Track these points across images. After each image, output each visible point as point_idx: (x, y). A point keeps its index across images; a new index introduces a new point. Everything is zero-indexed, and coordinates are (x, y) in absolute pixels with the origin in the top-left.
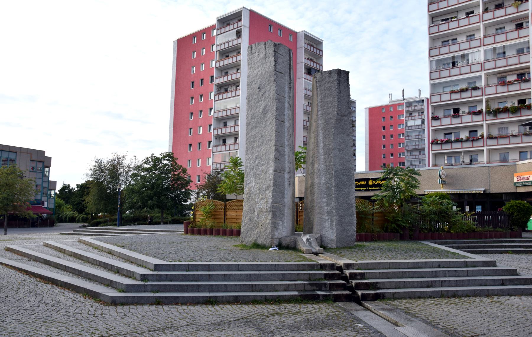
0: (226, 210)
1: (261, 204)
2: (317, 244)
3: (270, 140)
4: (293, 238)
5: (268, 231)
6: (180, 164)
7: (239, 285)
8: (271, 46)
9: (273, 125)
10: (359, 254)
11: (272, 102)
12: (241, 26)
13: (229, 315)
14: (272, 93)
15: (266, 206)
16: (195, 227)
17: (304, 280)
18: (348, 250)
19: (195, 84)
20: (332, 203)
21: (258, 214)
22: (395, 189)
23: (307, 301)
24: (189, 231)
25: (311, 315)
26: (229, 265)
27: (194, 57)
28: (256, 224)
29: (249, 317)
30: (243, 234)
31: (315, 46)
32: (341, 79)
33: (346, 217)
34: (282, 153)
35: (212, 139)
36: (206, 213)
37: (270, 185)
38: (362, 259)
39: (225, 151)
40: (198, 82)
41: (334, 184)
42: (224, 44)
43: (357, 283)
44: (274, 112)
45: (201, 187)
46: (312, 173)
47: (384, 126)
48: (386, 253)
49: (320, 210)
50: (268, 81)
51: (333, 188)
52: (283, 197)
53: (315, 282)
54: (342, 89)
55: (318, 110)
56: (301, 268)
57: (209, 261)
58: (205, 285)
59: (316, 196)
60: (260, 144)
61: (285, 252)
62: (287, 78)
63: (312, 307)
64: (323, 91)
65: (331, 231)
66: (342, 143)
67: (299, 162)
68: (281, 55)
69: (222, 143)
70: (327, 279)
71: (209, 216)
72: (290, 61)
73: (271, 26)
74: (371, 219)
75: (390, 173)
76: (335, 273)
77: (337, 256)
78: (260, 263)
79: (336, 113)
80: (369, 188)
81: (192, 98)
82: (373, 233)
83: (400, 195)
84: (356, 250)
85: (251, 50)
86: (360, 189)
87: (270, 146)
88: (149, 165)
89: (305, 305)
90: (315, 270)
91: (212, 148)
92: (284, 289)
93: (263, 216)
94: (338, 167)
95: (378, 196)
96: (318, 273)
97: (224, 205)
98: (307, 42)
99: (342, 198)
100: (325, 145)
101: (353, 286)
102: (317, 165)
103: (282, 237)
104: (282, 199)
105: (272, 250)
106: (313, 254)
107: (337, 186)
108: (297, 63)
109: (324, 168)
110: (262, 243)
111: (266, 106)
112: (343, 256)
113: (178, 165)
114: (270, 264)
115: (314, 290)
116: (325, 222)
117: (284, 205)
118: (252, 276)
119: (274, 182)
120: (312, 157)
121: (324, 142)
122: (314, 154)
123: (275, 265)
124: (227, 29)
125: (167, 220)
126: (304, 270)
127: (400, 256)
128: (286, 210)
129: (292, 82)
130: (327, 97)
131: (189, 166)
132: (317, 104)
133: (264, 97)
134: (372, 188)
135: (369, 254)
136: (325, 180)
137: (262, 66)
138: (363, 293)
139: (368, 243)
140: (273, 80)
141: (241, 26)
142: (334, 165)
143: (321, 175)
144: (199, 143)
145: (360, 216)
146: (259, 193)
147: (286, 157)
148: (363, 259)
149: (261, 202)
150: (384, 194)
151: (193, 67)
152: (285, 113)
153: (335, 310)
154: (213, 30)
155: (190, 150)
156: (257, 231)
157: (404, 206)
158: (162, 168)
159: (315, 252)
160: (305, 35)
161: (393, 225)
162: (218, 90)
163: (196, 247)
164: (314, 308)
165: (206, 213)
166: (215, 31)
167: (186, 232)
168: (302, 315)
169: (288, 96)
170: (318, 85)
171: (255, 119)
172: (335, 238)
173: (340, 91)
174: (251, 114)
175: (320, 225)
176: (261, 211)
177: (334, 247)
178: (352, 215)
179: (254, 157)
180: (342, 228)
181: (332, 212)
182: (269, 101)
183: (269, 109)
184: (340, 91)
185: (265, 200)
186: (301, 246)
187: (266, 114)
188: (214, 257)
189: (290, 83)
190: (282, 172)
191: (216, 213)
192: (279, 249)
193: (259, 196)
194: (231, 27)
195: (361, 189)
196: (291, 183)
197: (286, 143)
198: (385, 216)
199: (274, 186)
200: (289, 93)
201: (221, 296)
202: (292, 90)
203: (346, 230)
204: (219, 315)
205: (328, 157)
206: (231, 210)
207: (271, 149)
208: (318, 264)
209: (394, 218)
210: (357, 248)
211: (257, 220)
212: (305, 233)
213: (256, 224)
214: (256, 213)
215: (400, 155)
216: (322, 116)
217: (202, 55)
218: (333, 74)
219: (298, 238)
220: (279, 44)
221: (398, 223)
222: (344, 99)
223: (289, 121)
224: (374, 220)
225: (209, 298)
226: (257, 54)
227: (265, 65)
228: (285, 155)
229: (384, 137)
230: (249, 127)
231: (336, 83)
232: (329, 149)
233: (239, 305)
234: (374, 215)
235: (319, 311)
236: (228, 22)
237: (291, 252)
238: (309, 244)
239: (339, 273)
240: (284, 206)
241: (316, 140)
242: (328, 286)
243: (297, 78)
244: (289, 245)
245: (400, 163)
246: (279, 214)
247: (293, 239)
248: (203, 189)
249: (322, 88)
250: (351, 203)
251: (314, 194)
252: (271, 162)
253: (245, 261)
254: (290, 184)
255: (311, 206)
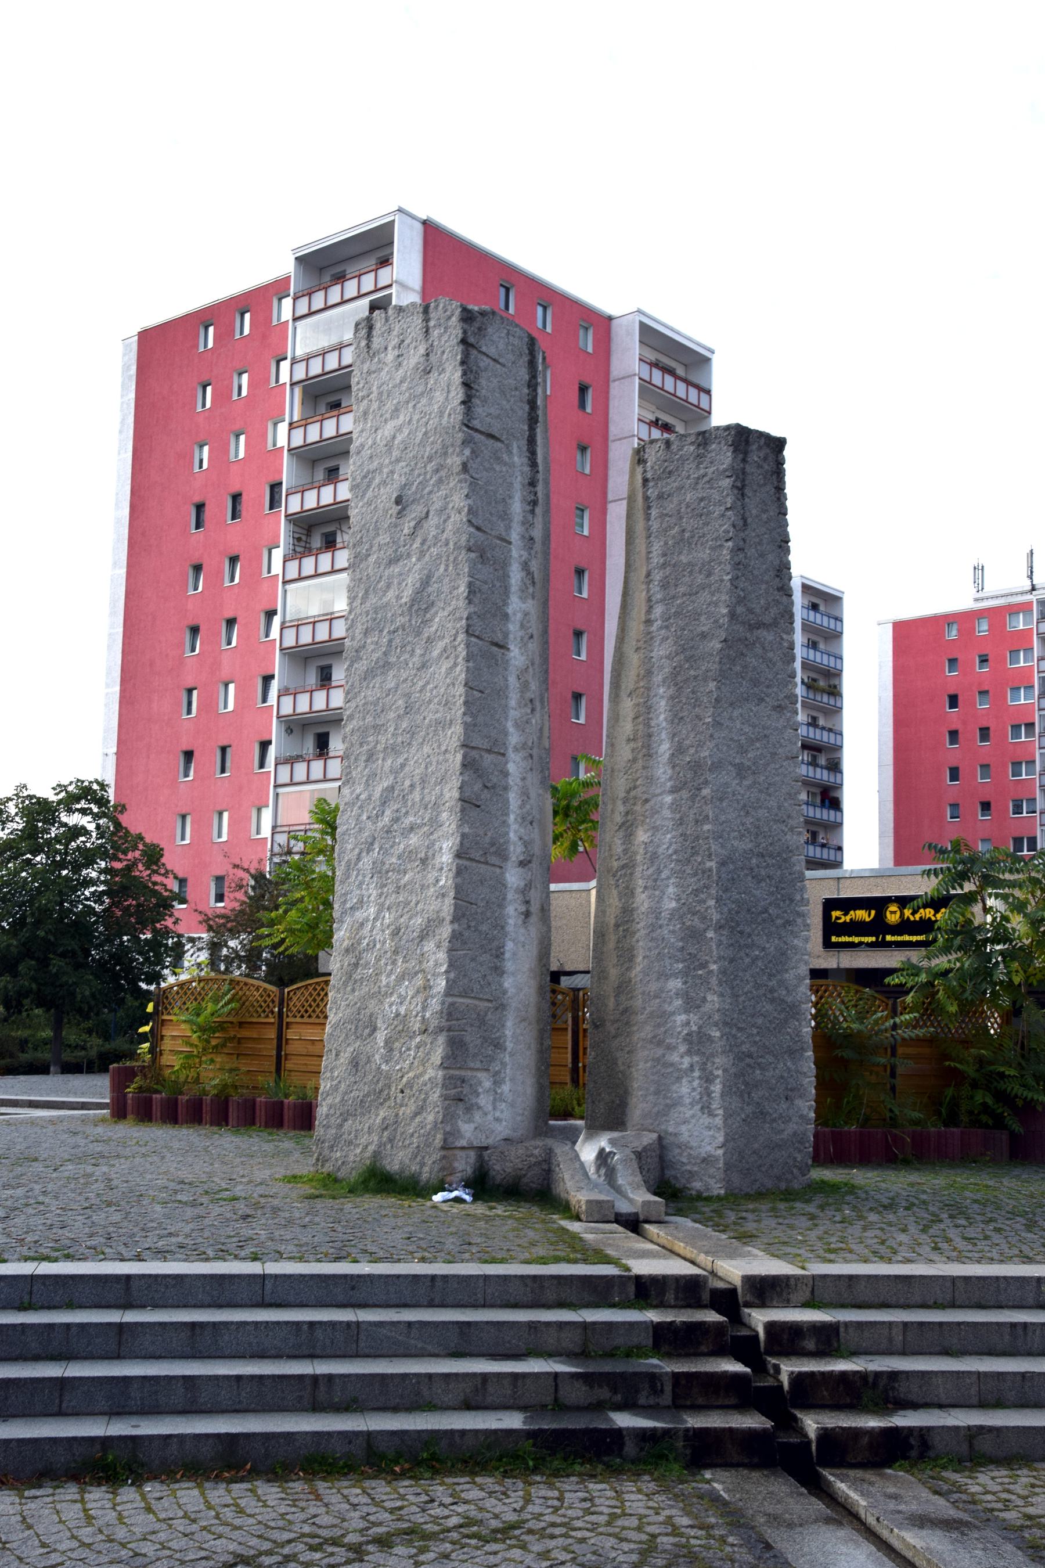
0: (286, 1020)
1: (400, 996)
2: (639, 1178)
3: (442, 724)
4: (536, 1147)
5: (431, 1118)
6: (134, 830)
7: (252, 1377)
8: (449, 318)
9: (457, 657)
10: (819, 1231)
11: (451, 559)
12: (390, 286)
13: (174, 1545)
14: (455, 522)
15: (424, 1008)
16: (157, 1092)
17: (561, 1355)
18: (773, 1209)
19: (208, 513)
20: (709, 998)
21: (386, 1042)
22: (986, 941)
23: (565, 1459)
24: (129, 1108)
25: (565, 1549)
26: (223, 1277)
27: (204, 405)
28: (380, 1085)
29: (269, 1553)
30: (327, 1127)
31: (680, 371)
32: (748, 469)
33: (771, 1059)
34: (495, 780)
35: (275, 732)
36: (202, 1029)
37: (442, 915)
38: (830, 1254)
39: (325, 780)
40: (219, 508)
41: (716, 917)
42: (323, 354)
43: (800, 1374)
44: (462, 603)
45: (222, 921)
46: (623, 867)
47: (952, 692)
48: (942, 1226)
49: (659, 1025)
50: (437, 471)
51: (710, 934)
52: (499, 971)
53: (608, 1367)
54: (754, 512)
55: (649, 600)
56: (550, 1296)
57: (139, 1258)
58: (93, 1379)
59: (638, 969)
60: (400, 739)
61: (500, 1210)
62: (518, 459)
63: (581, 1495)
64: (673, 520)
65: (706, 1120)
66: (752, 741)
67: (583, 822)
68: (495, 360)
69: (311, 751)
70: (665, 1348)
71: (214, 1042)
72: (535, 390)
73: (507, 290)
74: (885, 1067)
75: (963, 876)
76: (701, 1325)
77: (724, 1236)
78: (365, 1268)
79: (725, 611)
80: (889, 938)
81: (198, 569)
82: (894, 1131)
83: (1006, 967)
84: (811, 1208)
85: (369, 336)
86: (850, 939)
87: (443, 748)
88: (7, 831)
89: (551, 1486)
90: (613, 1306)
91: (272, 769)
92: (461, 1397)
93: (409, 1049)
94: (736, 843)
95: (916, 971)
96: (624, 1323)
97: (277, 1000)
98: (652, 356)
99: (752, 976)
100: (679, 750)
101: (781, 1387)
102: (646, 831)
103: (490, 1141)
104: (490, 978)
105: (445, 1202)
106: (617, 1221)
107: (730, 925)
108: (611, 438)
109: (674, 847)
110: (402, 1170)
111: (429, 577)
112: (746, 1238)
113: (127, 832)
114: (406, 1276)
115: (599, 1407)
116: (679, 1079)
117: (502, 1005)
118: (319, 1333)
119: (456, 905)
120: (625, 801)
121: (674, 735)
122: (635, 788)
123: (433, 1278)
124: (335, 294)
125: (83, 1053)
126: (561, 1305)
127: (1004, 1246)
128: (509, 1024)
129: (540, 476)
130: (690, 544)
131: (183, 839)
132: (648, 575)
133: (419, 540)
134: (899, 938)
135: (865, 1229)
136: (678, 900)
137: (411, 405)
138: (826, 1429)
139: (870, 1175)
140: (457, 468)
141: (390, 286)
142: (718, 836)
143: (663, 876)
144: (224, 750)
145: (838, 1052)
146: (396, 952)
147: (513, 798)
148: (832, 1256)
149: (402, 991)
150: (942, 962)
151: (201, 447)
152: (510, 610)
153: (685, 1521)
154: (280, 300)
155: (186, 775)
156: (382, 1114)
157: (1024, 1015)
158: (59, 842)
159: (630, 1214)
160: (644, 327)
161: (981, 1097)
162: (299, 539)
163: (115, 1183)
164: (591, 1500)
165: (202, 1029)
166: (287, 303)
167: (119, 1111)
168: (524, 1547)
169: (523, 537)
170: (652, 493)
171: (381, 631)
172: (720, 1152)
173: (745, 520)
174: (367, 613)
175: (657, 1093)
176: (401, 1028)
177: (715, 1193)
178: (794, 1053)
179: (377, 794)
180: (749, 1110)
181: (710, 1039)
182: (439, 556)
183: (439, 592)
184: (745, 520)
185: (419, 981)
186: (569, 1184)
187: (426, 610)
188: (170, 1235)
189: (532, 483)
190: (493, 860)
191: (245, 1033)
192: (476, 1198)
193: (394, 962)
194: (351, 288)
195: (856, 940)
196: (535, 908)
197: (514, 738)
198: (946, 1057)
199: (455, 919)
200: (528, 524)
201: (159, 1436)
202: (538, 510)
203: (768, 1119)
204: (123, 1545)
205: (693, 798)
206: (306, 1020)
207: (447, 761)
208: (629, 1278)
209: (981, 1067)
210: (819, 1200)
211: (383, 1067)
212: (595, 1128)
213: (380, 1085)
214: (380, 1037)
215: (1018, 809)
216: (667, 627)
217: (235, 397)
218: (713, 446)
219: (561, 1150)
220: (483, 314)
221: (1002, 1086)
222: (762, 555)
223: (524, 645)
224: (899, 1071)
225: (98, 1447)
226: (391, 356)
227: (424, 401)
228: (506, 788)
229: (954, 735)
230: (356, 665)
231: (726, 483)
232: (696, 766)
233: (242, 1480)
234: (900, 1051)
235: (613, 1517)
236: (338, 269)
237: (523, 1210)
238: (606, 1175)
239: (719, 1323)
240: (502, 1007)
241: (641, 727)
242: (668, 1388)
243: (610, 497)
244: (520, 1178)
245: (1018, 842)
246: (479, 1042)
247: (536, 1152)
248: (230, 930)
249: (671, 506)
250: (789, 999)
251: (631, 959)
252: (445, 815)
253: (301, 1259)
254: (527, 914)
255: (621, 1008)
